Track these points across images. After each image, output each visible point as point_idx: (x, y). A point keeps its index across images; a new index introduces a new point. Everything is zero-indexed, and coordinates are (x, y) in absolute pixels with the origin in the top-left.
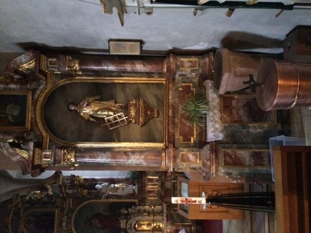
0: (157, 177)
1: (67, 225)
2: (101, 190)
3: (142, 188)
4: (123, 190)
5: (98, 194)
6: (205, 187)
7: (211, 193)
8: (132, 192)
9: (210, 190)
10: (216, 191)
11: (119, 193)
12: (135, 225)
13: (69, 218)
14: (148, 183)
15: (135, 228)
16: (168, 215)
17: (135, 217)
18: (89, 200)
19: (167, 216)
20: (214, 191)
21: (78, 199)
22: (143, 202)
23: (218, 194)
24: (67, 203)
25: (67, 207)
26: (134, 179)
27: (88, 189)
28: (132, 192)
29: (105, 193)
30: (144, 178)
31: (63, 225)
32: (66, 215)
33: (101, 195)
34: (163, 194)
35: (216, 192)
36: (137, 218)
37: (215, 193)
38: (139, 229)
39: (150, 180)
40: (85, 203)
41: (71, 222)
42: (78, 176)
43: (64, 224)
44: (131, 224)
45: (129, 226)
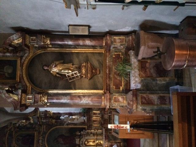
0: (99, 112)
1: (42, 142)
2: (64, 120)
3: (89, 119)
4: (77, 120)
5: (62, 123)
6: (129, 118)
7: (133, 122)
8: (83, 121)
9: (132, 120)
10: (136, 120)
11: (75, 122)
12: (85, 142)
13: (44, 138)
14: (93, 116)
15: (85, 144)
16: (106, 135)
17: (85, 137)
18: (56, 126)
19: (105, 136)
20: (135, 120)
21: (49, 126)
22: (90, 127)
23: (138, 123)
24: (43, 128)
25: (42, 131)
26: (84, 113)
27: (56, 119)
28: (83, 121)
29: (66, 122)
30: (91, 113)
31: (40, 142)
32: (42, 136)
33: (63, 123)
34: (103, 122)
35: (136, 121)
36: (86, 138)
37: (135, 122)
38: (88, 144)
39: (95, 114)
40: (54, 128)
41: (44, 140)
42: (49, 111)
43: (40, 141)
44: (83, 141)
45: (81, 143)
